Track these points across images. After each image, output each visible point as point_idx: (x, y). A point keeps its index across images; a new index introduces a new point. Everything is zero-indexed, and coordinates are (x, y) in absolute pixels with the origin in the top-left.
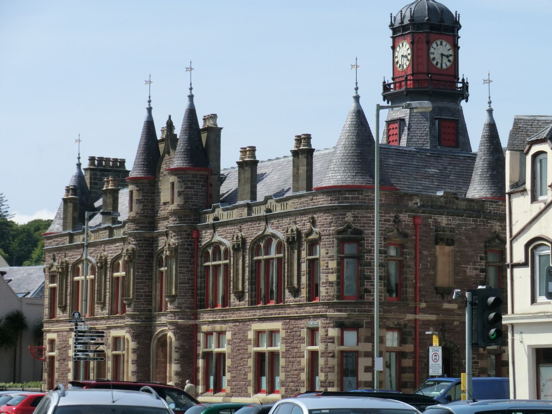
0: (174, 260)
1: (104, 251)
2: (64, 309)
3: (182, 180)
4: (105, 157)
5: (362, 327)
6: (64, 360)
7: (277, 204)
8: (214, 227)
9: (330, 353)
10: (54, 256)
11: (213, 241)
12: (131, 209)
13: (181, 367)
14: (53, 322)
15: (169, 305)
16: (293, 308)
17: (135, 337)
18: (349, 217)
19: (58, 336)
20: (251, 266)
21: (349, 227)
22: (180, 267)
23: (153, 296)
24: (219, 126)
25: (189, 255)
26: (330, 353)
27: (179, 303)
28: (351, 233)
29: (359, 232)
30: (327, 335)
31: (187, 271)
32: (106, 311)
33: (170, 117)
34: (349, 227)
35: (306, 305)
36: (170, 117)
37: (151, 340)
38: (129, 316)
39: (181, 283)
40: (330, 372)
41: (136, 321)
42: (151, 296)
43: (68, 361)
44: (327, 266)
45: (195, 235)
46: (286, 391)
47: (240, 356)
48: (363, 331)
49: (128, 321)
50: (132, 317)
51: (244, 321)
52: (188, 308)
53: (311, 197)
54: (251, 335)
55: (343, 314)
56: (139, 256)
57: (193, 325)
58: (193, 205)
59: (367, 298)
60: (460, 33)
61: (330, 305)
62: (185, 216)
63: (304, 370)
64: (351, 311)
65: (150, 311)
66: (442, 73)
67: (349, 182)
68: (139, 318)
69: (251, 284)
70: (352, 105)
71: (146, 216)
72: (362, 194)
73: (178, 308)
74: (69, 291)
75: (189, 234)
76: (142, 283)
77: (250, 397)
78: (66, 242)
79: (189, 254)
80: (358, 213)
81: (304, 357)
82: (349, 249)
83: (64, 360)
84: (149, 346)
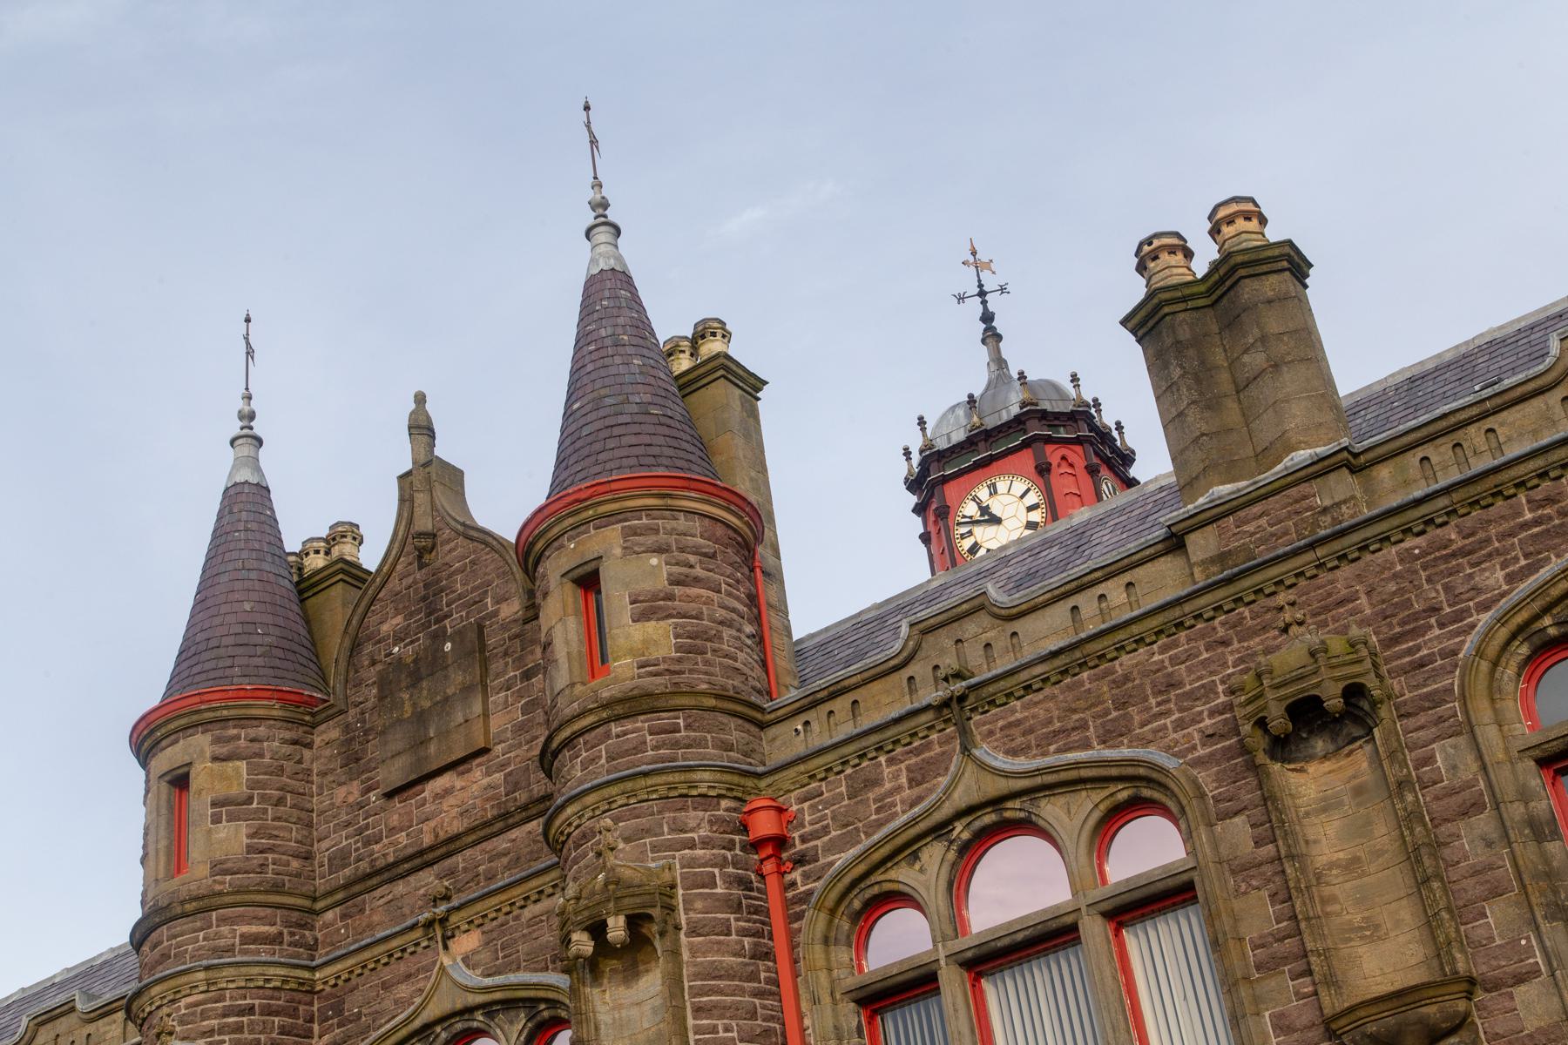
22: (699, 1010)
25: (747, 941)
33: (420, 399)
36: (420, 399)
79: (743, 933)
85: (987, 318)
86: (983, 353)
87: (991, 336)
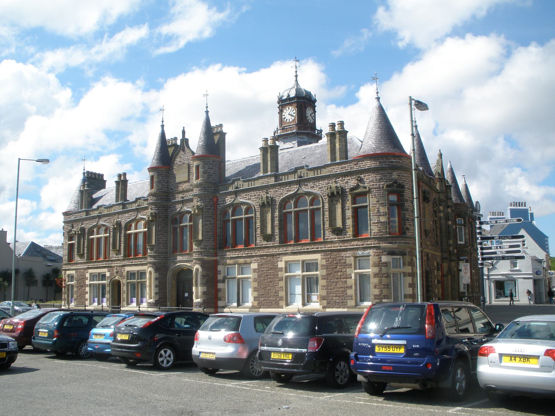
0: (201, 217)
1: (118, 218)
2: (81, 256)
3: (205, 164)
4: (94, 172)
5: (405, 255)
6: (82, 286)
7: (308, 172)
8: (237, 193)
9: (384, 274)
10: (72, 225)
11: (299, 192)
12: (152, 187)
13: (207, 289)
14: (403, 237)
15: (149, 251)
16: (336, 243)
17: (157, 270)
18: (395, 175)
19: (76, 272)
20: (280, 216)
21: (395, 182)
23: (169, 244)
24: (224, 131)
26: (384, 274)
27: (204, 246)
28: (397, 187)
29: (402, 186)
30: (381, 261)
31: (210, 224)
32: (121, 256)
34: (395, 182)
35: (352, 240)
37: (167, 272)
38: (151, 256)
39: (205, 232)
40: (384, 288)
41: (389, 243)
42: (167, 243)
43: (85, 287)
44: (379, 211)
45: (215, 200)
46: (328, 304)
47: (269, 280)
48: (408, 258)
49: (149, 260)
50: (154, 257)
51: (273, 255)
52: (211, 249)
53: (356, 163)
54: (281, 265)
55: (395, 246)
56: (159, 217)
57: (214, 260)
58: (213, 180)
59: (409, 234)
60: (316, 104)
61: (380, 239)
62: (208, 187)
63: (351, 287)
64: (400, 243)
65: (166, 253)
66: (311, 124)
67: (385, 151)
68: (159, 257)
69: (280, 229)
70: (375, 103)
71: (164, 192)
72: (401, 160)
73: (156, 253)
74: (86, 245)
75: (211, 199)
76: (161, 234)
77: (283, 308)
78: (84, 215)
80: (400, 173)
81: (351, 278)
82: (393, 198)
83: (82, 286)
84: (165, 276)
85: (296, 72)
86: (295, 78)
87: (296, 76)
